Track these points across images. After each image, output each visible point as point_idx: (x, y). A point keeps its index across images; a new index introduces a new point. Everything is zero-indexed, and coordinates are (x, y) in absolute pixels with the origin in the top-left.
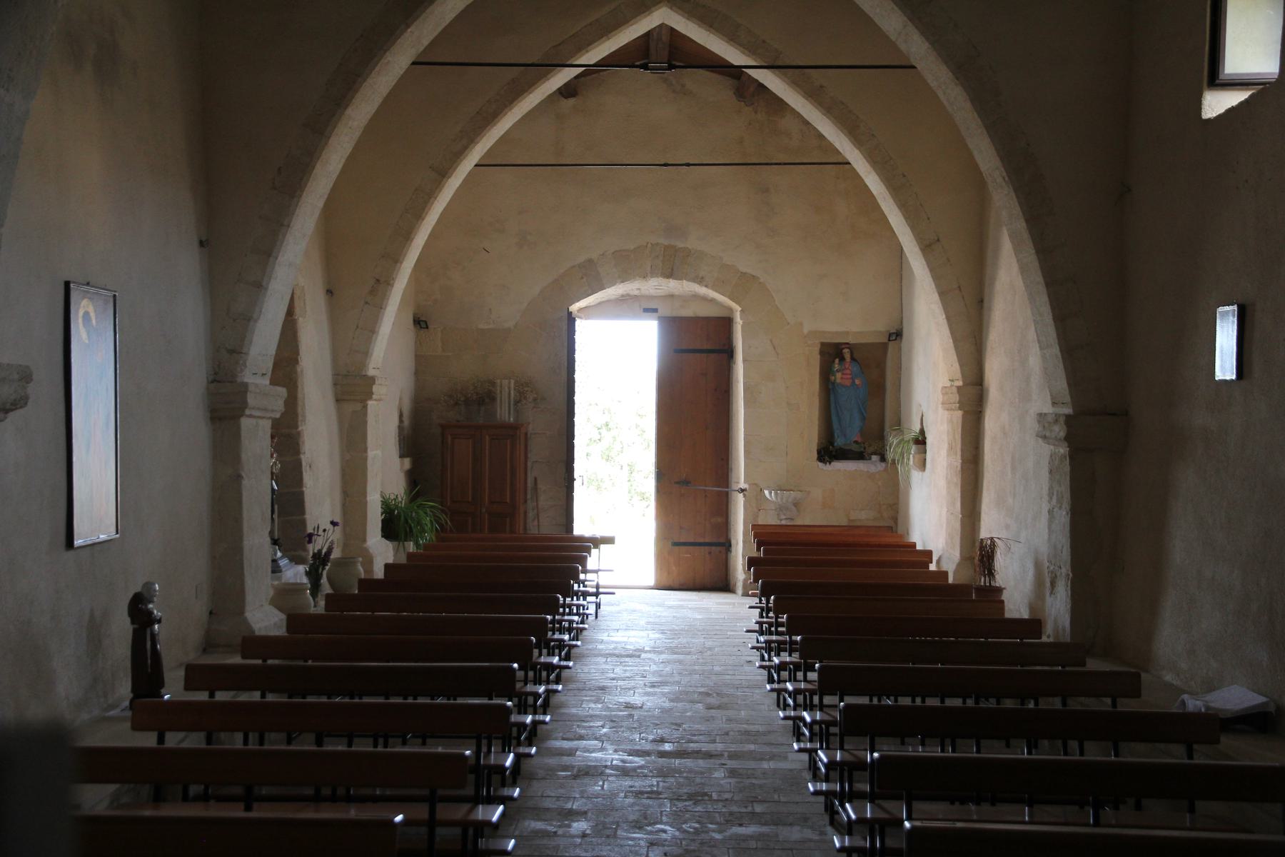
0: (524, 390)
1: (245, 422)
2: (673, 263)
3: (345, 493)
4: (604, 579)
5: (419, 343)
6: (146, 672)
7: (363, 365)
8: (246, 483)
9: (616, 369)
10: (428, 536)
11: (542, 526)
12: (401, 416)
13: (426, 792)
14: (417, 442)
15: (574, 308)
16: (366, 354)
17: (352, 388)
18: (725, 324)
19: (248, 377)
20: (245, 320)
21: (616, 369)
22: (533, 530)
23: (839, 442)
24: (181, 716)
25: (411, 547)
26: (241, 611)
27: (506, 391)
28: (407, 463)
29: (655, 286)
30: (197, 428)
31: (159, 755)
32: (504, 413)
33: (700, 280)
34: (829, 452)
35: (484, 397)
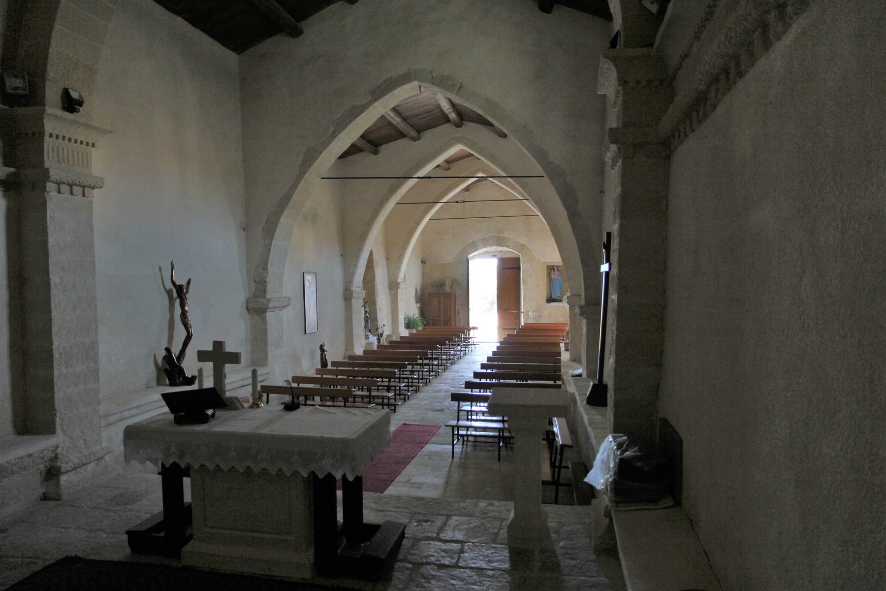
0: (454, 282)
1: (353, 301)
2: (500, 242)
3: (392, 316)
4: (475, 340)
5: (423, 268)
6: (324, 363)
7: (397, 279)
8: (354, 316)
9: (483, 275)
10: (420, 328)
11: (461, 324)
12: (416, 291)
13: (501, 418)
14: (423, 299)
15: (470, 256)
16: (398, 276)
17: (393, 286)
18: (519, 259)
19: (354, 289)
20: (353, 274)
21: (483, 275)
22: (458, 325)
23: (554, 297)
24: (330, 372)
25: (414, 331)
26: (353, 349)
27: (448, 283)
28: (418, 305)
29: (495, 248)
30: (340, 303)
31: (322, 378)
32: (448, 289)
33: (508, 247)
34: (550, 300)
35: (442, 285)
